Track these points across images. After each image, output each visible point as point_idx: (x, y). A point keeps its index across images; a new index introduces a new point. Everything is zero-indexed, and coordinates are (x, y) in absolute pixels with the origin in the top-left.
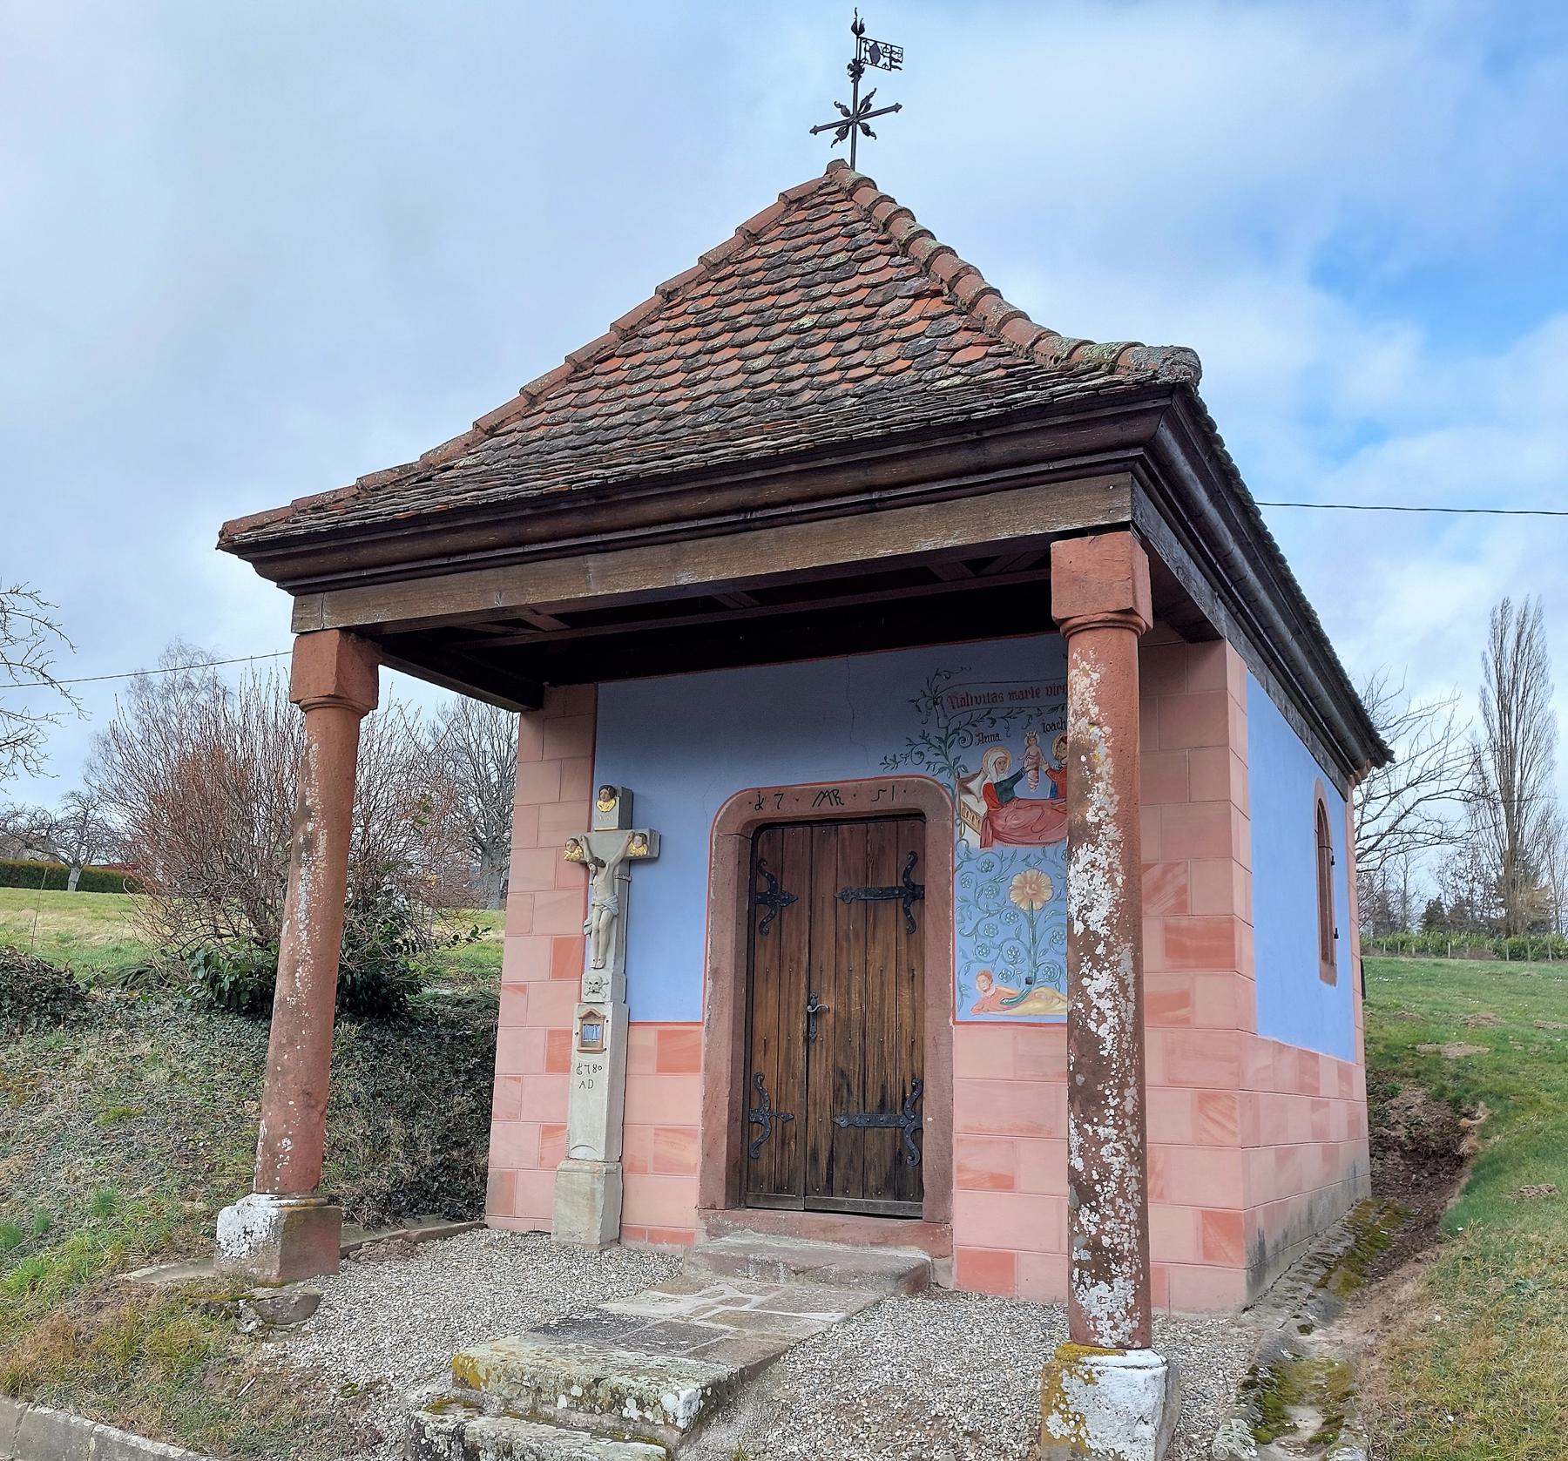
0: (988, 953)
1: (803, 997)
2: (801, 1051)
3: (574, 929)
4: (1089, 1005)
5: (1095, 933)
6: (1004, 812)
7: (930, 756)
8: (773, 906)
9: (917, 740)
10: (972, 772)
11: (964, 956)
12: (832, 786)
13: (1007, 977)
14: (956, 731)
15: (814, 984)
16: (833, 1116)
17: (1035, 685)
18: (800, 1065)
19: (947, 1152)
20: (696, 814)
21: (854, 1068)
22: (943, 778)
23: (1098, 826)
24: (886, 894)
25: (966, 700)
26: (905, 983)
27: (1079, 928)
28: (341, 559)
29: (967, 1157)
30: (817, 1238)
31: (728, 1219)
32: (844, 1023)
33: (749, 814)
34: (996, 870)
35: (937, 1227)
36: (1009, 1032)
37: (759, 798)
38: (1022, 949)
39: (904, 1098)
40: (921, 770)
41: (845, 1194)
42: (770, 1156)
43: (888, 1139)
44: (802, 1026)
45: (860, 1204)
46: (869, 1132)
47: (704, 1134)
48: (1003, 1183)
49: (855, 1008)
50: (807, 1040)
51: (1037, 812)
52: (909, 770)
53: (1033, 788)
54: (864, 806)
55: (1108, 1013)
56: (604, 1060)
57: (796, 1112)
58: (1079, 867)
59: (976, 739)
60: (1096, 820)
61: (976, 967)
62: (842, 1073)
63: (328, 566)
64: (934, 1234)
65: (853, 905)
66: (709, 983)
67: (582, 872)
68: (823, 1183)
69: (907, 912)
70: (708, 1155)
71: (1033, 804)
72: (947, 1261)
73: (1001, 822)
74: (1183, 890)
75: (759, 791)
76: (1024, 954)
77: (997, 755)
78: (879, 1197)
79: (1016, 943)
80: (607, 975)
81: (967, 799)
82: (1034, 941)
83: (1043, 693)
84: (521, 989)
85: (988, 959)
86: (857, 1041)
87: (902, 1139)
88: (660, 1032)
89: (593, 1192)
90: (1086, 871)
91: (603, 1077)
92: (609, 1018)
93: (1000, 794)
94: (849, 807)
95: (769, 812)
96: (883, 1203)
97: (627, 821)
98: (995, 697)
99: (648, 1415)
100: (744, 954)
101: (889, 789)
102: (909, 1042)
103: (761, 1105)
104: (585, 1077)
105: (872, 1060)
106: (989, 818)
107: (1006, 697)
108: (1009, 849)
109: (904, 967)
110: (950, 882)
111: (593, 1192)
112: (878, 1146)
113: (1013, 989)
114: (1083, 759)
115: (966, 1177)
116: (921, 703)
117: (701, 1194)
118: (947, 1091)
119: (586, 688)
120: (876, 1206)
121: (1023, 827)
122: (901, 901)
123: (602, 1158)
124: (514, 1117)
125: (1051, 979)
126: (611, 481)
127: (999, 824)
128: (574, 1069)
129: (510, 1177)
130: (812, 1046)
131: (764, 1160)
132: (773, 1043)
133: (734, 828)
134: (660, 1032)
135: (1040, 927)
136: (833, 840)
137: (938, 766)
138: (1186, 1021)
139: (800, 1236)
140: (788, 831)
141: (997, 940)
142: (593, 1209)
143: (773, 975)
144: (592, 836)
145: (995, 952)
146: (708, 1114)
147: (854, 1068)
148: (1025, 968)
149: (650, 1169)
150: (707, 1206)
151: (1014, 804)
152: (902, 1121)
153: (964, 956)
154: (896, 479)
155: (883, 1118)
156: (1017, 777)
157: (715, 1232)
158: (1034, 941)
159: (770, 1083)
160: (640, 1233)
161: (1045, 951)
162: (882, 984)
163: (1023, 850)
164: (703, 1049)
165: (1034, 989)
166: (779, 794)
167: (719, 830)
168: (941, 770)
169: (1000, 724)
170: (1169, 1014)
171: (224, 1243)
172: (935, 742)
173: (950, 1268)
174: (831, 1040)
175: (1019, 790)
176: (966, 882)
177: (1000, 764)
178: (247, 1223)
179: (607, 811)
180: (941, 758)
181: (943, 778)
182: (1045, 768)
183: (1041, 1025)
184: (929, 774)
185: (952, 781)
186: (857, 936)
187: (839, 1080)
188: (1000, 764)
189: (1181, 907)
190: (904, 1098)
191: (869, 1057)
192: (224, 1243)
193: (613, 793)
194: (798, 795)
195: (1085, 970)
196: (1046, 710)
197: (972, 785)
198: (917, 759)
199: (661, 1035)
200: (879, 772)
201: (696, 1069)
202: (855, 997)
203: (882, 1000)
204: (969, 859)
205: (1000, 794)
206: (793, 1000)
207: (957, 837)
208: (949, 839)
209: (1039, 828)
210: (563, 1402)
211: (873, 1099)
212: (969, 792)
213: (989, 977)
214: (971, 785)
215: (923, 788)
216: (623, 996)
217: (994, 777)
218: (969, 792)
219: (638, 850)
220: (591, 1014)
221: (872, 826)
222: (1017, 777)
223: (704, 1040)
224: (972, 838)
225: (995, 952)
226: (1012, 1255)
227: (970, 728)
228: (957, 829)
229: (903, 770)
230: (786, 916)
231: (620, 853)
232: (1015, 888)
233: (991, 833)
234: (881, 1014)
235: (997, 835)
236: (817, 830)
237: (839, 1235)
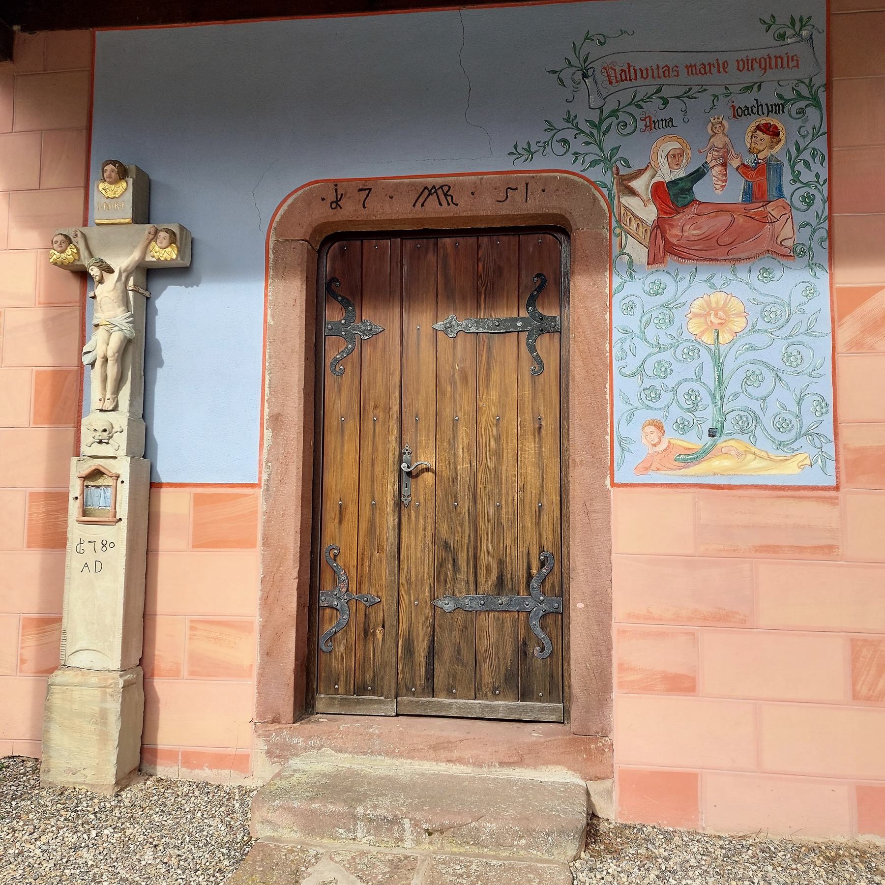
0: (658, 397)
1: (393, 454)
2: (390, 518)
6: (680, 219)
7: (577, 145)
8: (351, 338)
9: (560, 124)
10: (636, 166)
11: (627, 402)
12: (440, 181)
13: (683, 427)
14: (614, 113)
15: (407, 437)
16: (433, 598)
17: (722, 58)
18: (389, 535)
19: (603, 647)
20: (248, 203)
21: (461, 539)
22: (596, 174)
25: (627, 74)
26: (530, 437)
29: (630, 653)
30: (425, 758)
31: (297, 735)
32: (449, 486)
33: (321, 214)
35: (590, 743)
36: (687, 496)
37: (337, 193)
39: (530, 576)
40: (566, 163)
41: (450, 694)
42: (349, 649)
43: (508, 625)
44: (391, 488)
45: (472, 707)
47: (264, 628)
48: (681, 684)
50: (399, 505)
51: (726, 219)
53: (721, 189)
54: (486, 208)
56: (119, 534)
57: (384, 594)
59: (641, 125)
62: (446, 545)
64: (588, 752)
65: (459, 340)
66: (268, 434)
67: (74, 285)
68: (421, 681)
69: (532, 348)
70: (268, 653)
71: (720, 209)
72: (608, 783)
73: (676, 231)
75: (336, 183)
76: (707, 399)
77: (672, 145)
78: (496, 696)
79: (696, 386)
80: (120, 420)
81: (628, 201)
82: (720, 382)
83: (732, 67)
85: (658, 405)
86: (464, 507)
87: (528, 628)
89: (104, 714)
91: (118, 558)
92: (125, 476)
93: (673, 197)
94: (465, 208)
95: (350, 212)
96: (504, 705)
97: (143, 213)
98: (667, 71)
100: (312, 398)
101: (521, 187)
102: (535, 508)
103: (335, 586)
104: (89, 557)
105: (486, 529)
106: (660, 226)
107: (683, 71)
109: (528, 416)
111: (104, 714)
112: (494, 638)
113: (694, 441)
115: (632, 677)
116: (566, 75)
117: (259, 704)
118: (602, 569)
119: (76, 37)
120: (493, 708)
121: (706, 238)
122: (524, 336)
123: (117, 665)
125: (743, 430)
127: (674, 234)
128: (72, 545)
130: (405, 512)
131: (340, 655)
132: (352, 508)
133: (301, 231)
135: (729, 365)
136: (431, 257)
137: (589, 159)
139: (401, 755)
140: (371, 245)
141: (671, 382)
142: (103, 738)
143: (351, 425)
144: (90, 231)
146: (267, 602)
147: (461, 539)
148: (709, 416)
149: (185, 671)
150: (268, 718)
151: (694, 209)
152: (529, 604)
153: (627, 402)
155: (504, 599)
156: (698, 175)
157: (278, 753)
158: (720, 382)
159: (348, 557)
160: (172, 755)
161: (736, 395)
162: (499, 437)
164: (261, 519)
165: (721, 442)
166: (366, 188)
167: (278, 235)
168: (594, 163)
169: (675, 107)
173: (609, 792)
174: (431, 505)
175: (700, 191)
176: (629, 308)
177: (675, 158)
179: (113, 197)
180: (594, 148)
181: (596, 174)
182: (735, 163)
183: (730, 487)
184: (577, 168)
185: (608, 178)
186: (465, 379)
188: (675, 158)
190: (530, 576)
191: (481, 525)
193: (123, 173)
194: (393, 190)
197: (638, 184)
198: (559, 148)
199: (199, 501)
200: (508, 164)
201: (246, 543)
202: (462, 452)
203: (499, 455)
205: (673, 197)
206: (379, 457)
207: (616, 250)
209: (727, 240)
211: (488, 577)
212: (633, 192)
213: (659, 427)
214: (636, 184)
215: (569, 187)
216: (143, 448)
217: (666, 175)
218: (633, 192)
219: (164, 253)
220: (97, 474)
221: (485, 240)
223: (262, 506)
225: (667, 397)
226: (695, 775)
227: (632, 109)
228: (615, 241)
229: (539, 163)
230: (367, 351)
232: (697, 315)
234: (497, 473)
236: (409, 244)
237: (455, 754)
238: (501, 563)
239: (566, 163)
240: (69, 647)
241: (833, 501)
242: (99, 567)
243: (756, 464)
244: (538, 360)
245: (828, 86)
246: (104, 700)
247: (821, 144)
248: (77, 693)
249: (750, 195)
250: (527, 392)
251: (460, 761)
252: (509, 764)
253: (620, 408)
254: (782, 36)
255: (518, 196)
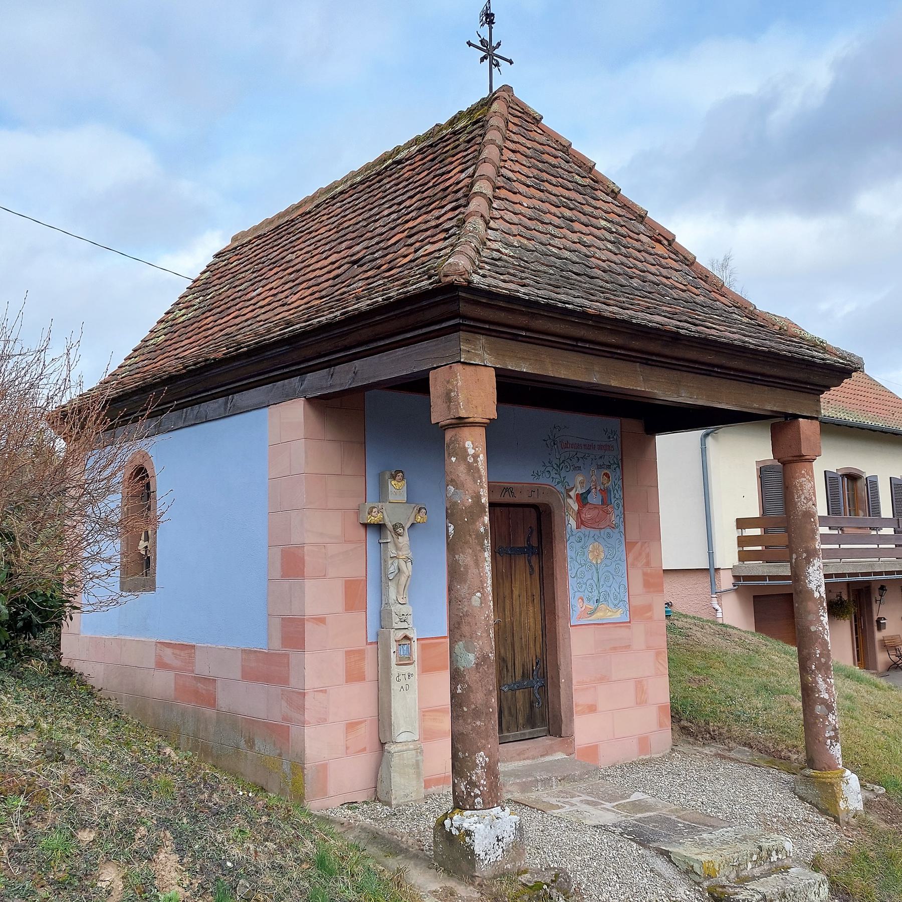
3: (359, 573)
7: (553, 474)
22: (559, 488)
24: (521, 551)
28: (522, 321)
29: (580, 698)
40: (549, 481)
41: (508, 731)
46: (517, 692)
48: (592, 709)
49: (508, 620)
52: (544, 480)
58: (815, 568)
61: (578, 595)
63: (511, 322)
74: (648, 555)
79: (591, 581)
81: (569, 501)
84: (321, 620)
88: (422, 645)
93: (582, 499)
99: (780, 856)
104: (403, 683)
109: (529, 594)
110: (565, 547)
113: (592, 606)
124: (322, 721)
126: (634, 321)
129: (323, 768)
134: (422, 645)
139: (508, 761)
147: (509, 656)
151: (587, 506)
156: (589, 492)
163: (593, 532)
165: (602, 606)
168: (558, 483)
171: (482, 854)
172: (555, 466)
178: (498, 832)
181: (559, 488)
182: (599, 488)
183: (603, 624)
185: (563, 490)
187: (502, 664)
189: (648, 564)
192: (482, 854)
196: (598, 457)
197: (572, 493)
200: (530, 480)
201: (445, 668)
202: (507, 613)
208: (564, 525)
210: (750, 866)
211: (519, 672)
212: (571, 497)
218: (571, 497)
222: (589, 492)
224: (573, 523)
225: (584, 586)
233: (581, 523)
237: (526, 756)
238: (523, 665)
239: (549, 481)
240: (395, 733)
241: (629, 627)
242: (407, 688)
243: (609, 614)
244: (531, 566)
245: (622, 459)
246: (417, 756)
247: (620, 482)
248: (405, 754)
249: (604, 502)
250: (529, 583)
251: (528, 758)
252: (547, 754)
253: (571, 592)
254: (609, 437)
255: (535, 494)
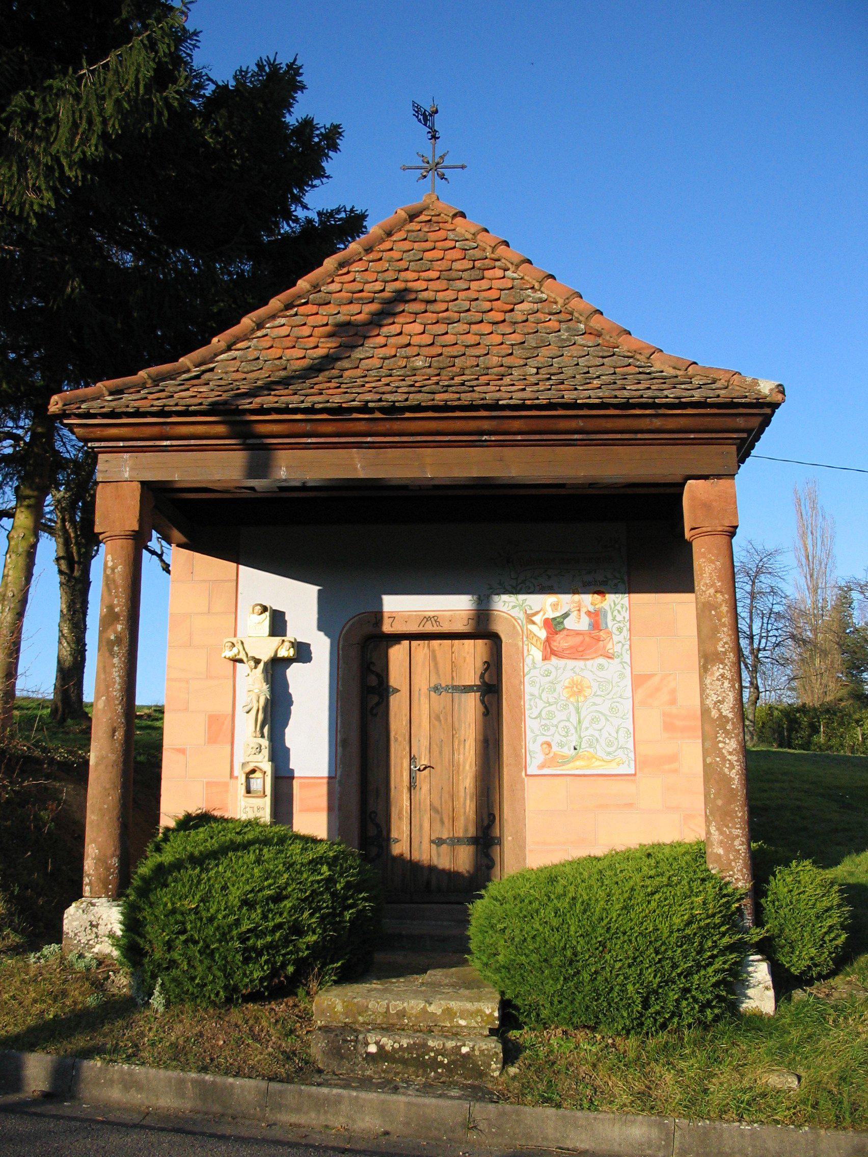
0: (549, 730)
4: (724, 759)
5: (725, 717)
11: (532, 731)
12: (433, 614)
23: (725, 653)
27: (714, 714)
34: (553, 676)
38: (572, 728)
55: (735, 763)
60: (723, 650)
73: (555, 644)
74: (673, 691)
76: (573, 730)
79: (567, 724)
81: (531, 627)
82: (579, 722)
84: (182, 751)
90: (718, 680)
106: (548, 640)
108: (561, 663)
114: (713, 612)
121: (571, 648)
127: (555, 645)
138: (676, 771)
141: (555, 722)
145: (553, 729)
151: (565, 632)
153: (532, 731)
154: (589, 420)
158: (579, 722)
161: (587, 728)
168: (514, 607)
170: (667, 767)
176: (533, 683)
195: (721, 739)
204: (535, 668)
209: (580, 649)
212: (534, 623)
214: (534, 619)
222: (566, 615)
224: (536, 654)
225: (553, 729)
228: (525, 648)
231: (271, 654)
235: (553, 653)
